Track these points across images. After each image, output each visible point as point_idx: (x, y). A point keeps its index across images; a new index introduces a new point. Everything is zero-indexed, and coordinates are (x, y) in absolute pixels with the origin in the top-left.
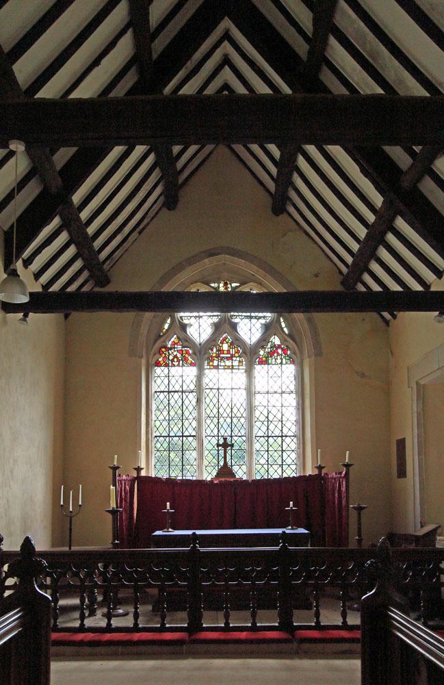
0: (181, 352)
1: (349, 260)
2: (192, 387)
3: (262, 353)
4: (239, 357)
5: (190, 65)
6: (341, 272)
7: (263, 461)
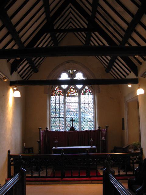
0: (59, 91)
1: (107, 64)
2: (62, 102)
3: (83, 91)
4: (76, 93)
5: (61, 16)
6: (105, 67)
7: (83, 125)
